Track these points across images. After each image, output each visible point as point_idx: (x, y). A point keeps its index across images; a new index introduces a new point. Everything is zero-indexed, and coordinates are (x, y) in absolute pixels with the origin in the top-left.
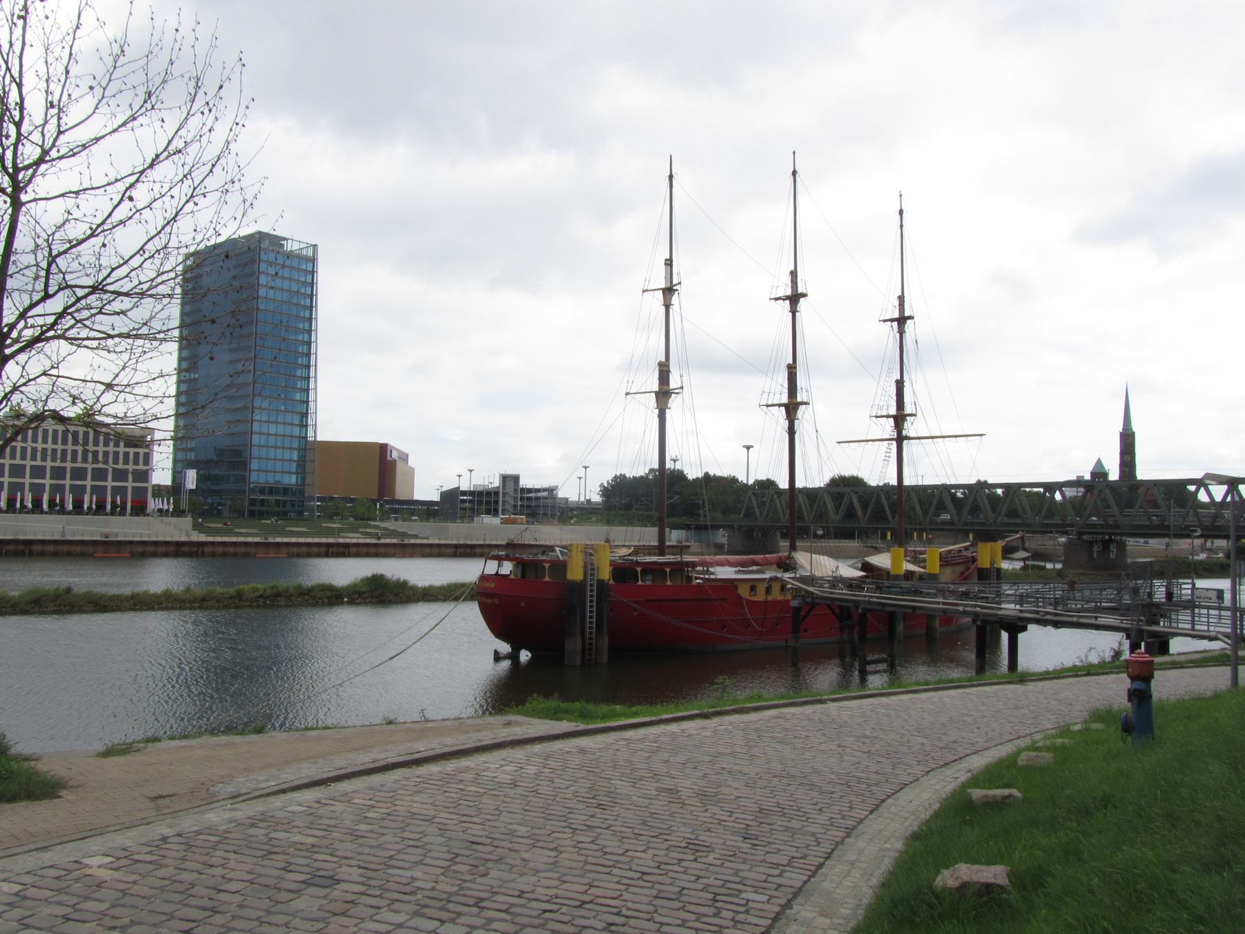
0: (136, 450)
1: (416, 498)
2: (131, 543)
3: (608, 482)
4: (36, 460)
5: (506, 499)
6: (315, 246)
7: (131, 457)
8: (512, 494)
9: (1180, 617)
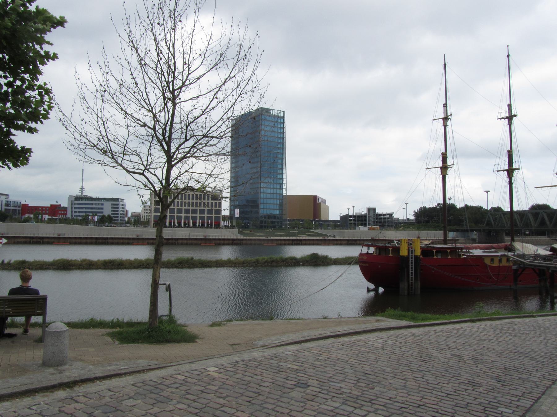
0: (216, 201)
2: (215, 239)
3: (418, 210)
5: (370, 219)
6: (284, 112)
7: (214, 204)
8: (373, 216)
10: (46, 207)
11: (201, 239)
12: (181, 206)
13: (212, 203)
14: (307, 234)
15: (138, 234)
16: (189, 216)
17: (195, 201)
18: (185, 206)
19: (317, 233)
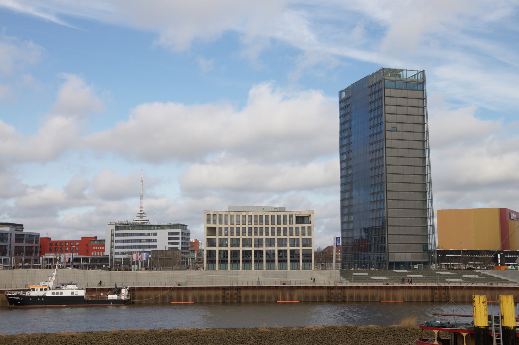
0: (303, 225)
1: (9, 228)
4: (292, 235)
6: (423, 72)
9: (427, 191)
10: (75, 242)
11: (277, 288)
12: (273, 234)
13: (297, 228)
14: (463, 278)
15: (179, 281)
16: (239, 250)
17: (282, 226)
18: (279, 234)
19: (484, 275)
